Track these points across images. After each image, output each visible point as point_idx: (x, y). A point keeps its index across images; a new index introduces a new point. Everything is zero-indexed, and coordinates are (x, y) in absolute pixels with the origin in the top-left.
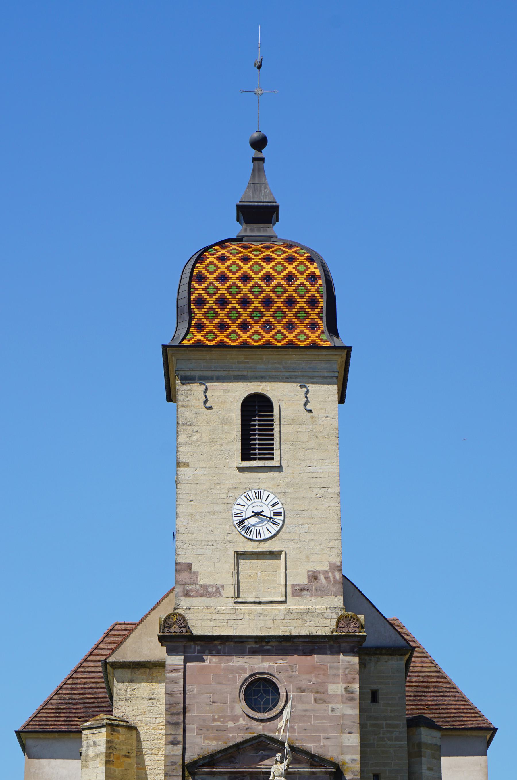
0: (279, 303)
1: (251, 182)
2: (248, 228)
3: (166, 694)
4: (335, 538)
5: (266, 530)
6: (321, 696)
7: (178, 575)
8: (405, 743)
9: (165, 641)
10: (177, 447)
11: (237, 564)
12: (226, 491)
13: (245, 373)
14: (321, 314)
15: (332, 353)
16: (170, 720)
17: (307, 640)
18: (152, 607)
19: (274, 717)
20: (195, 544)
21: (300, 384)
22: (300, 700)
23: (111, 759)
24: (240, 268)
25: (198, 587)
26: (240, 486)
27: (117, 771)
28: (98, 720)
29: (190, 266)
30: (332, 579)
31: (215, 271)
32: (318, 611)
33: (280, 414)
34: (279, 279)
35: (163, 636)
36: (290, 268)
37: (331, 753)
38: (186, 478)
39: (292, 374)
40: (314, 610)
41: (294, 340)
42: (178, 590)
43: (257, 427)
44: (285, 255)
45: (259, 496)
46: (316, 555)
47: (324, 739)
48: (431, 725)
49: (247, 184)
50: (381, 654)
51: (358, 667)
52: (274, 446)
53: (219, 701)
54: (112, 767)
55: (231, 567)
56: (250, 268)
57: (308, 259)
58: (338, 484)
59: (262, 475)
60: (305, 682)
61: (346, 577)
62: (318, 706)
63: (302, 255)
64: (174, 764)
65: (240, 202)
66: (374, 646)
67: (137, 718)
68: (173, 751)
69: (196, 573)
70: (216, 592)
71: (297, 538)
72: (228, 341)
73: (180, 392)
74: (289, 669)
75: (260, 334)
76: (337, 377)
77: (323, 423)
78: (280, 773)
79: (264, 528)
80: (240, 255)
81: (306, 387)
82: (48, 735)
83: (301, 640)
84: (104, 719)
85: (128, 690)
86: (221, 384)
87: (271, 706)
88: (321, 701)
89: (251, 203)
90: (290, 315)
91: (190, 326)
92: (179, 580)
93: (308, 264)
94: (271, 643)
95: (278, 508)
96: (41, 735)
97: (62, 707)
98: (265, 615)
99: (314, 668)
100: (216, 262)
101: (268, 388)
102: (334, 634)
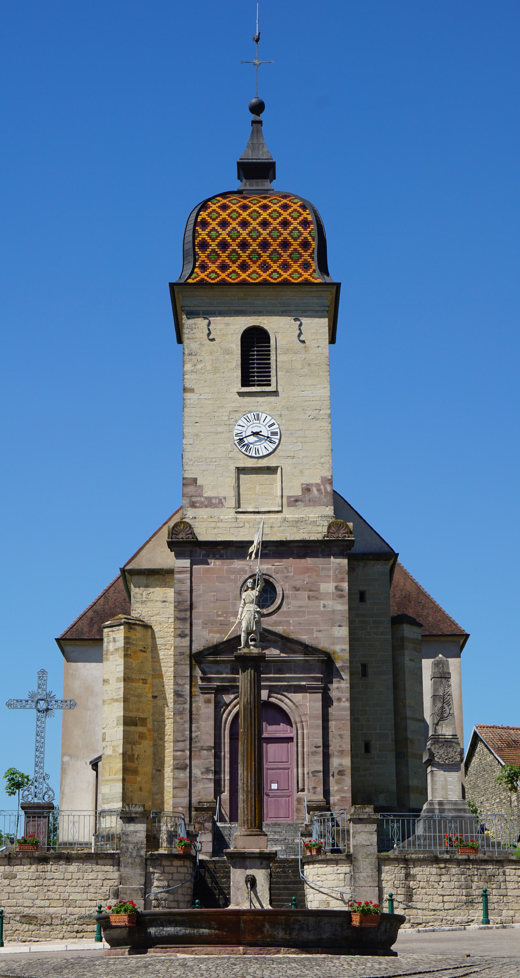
0: (275, 245)
1: (250, 143)
2: (248, 183)
3: (175, 593)
4: (326, 455)
5: (264, 448)
6: (314, 594)
7: (185, 489)
8: (389, 637)
9: (173, 546)
10: (184, 375)
11: (238, 479)
12: (228, 414)
13: (244, 308)
14: (313, 255)
16: (178, 616)
17: (301, 544)
18: (165, 522)
19: (272, 612)
20: (200, 461)
21: (294, 318)
22: (295, 597)
23: (129, 653)
24: (240, 215)
25: (203, 499)
26: (240, 409)
27: (134, 663)
28: (117, 619)
29: (194, 214)
30: (323, 491)
31: (217, 218)
32: (311, 519)
34: (275, 224)
35: (171, 542)
36: (285, 214)
37: (323, 644)
38: (191, 402)
39: (287, 308)
40: (307, 518)
41: (289, 278)
42: (186, 502)
43: (255, 357)
44: (280, 204)
45: (258, 418)
46: (309, 470)
47: (317, 631)
48: (413, 622)
49: (246, 145)
51: (347, 568)
52: (271, 374)
54: (130, 660)
55: (232, 481)
56: (249, 215)
57: (301, 206)
58: (328, 407)
59: (260, 399)
61: (336, 493)
62: (311, 603)
63: (295, 203)
64: (182, 654)
65: (240, 159)
66: (360, 551)
67: (152, 619)
68: (181, 642)
69: (201, 487)
70: (220, 503)
71: (292, 455)
72: (228, 279)
73: (186, 326)
74: (285, 571)
75: (257, 273)
76: (328, 311)
77: (315, 352)
78: (251, 599)
79: (262, 446)
80: (239, 204)
81: (299, 320)
82: (83, 643)
83: (296, 544)
84: (122, 619)
85: (144, 594)
86: (222, 318)
87: (269, 603)
88: (314, 599)
89: (250, 161)
90: (285, 256)
91: (194, 267)
92: (185, 493)
93: (301, 211)
94: (269, 548)
95: (275, 428)
96: (78, 643)
97: (96, 619)
99: (308, 570)
100: (218, 210)
101: (266, 322)
102: (326, 538)
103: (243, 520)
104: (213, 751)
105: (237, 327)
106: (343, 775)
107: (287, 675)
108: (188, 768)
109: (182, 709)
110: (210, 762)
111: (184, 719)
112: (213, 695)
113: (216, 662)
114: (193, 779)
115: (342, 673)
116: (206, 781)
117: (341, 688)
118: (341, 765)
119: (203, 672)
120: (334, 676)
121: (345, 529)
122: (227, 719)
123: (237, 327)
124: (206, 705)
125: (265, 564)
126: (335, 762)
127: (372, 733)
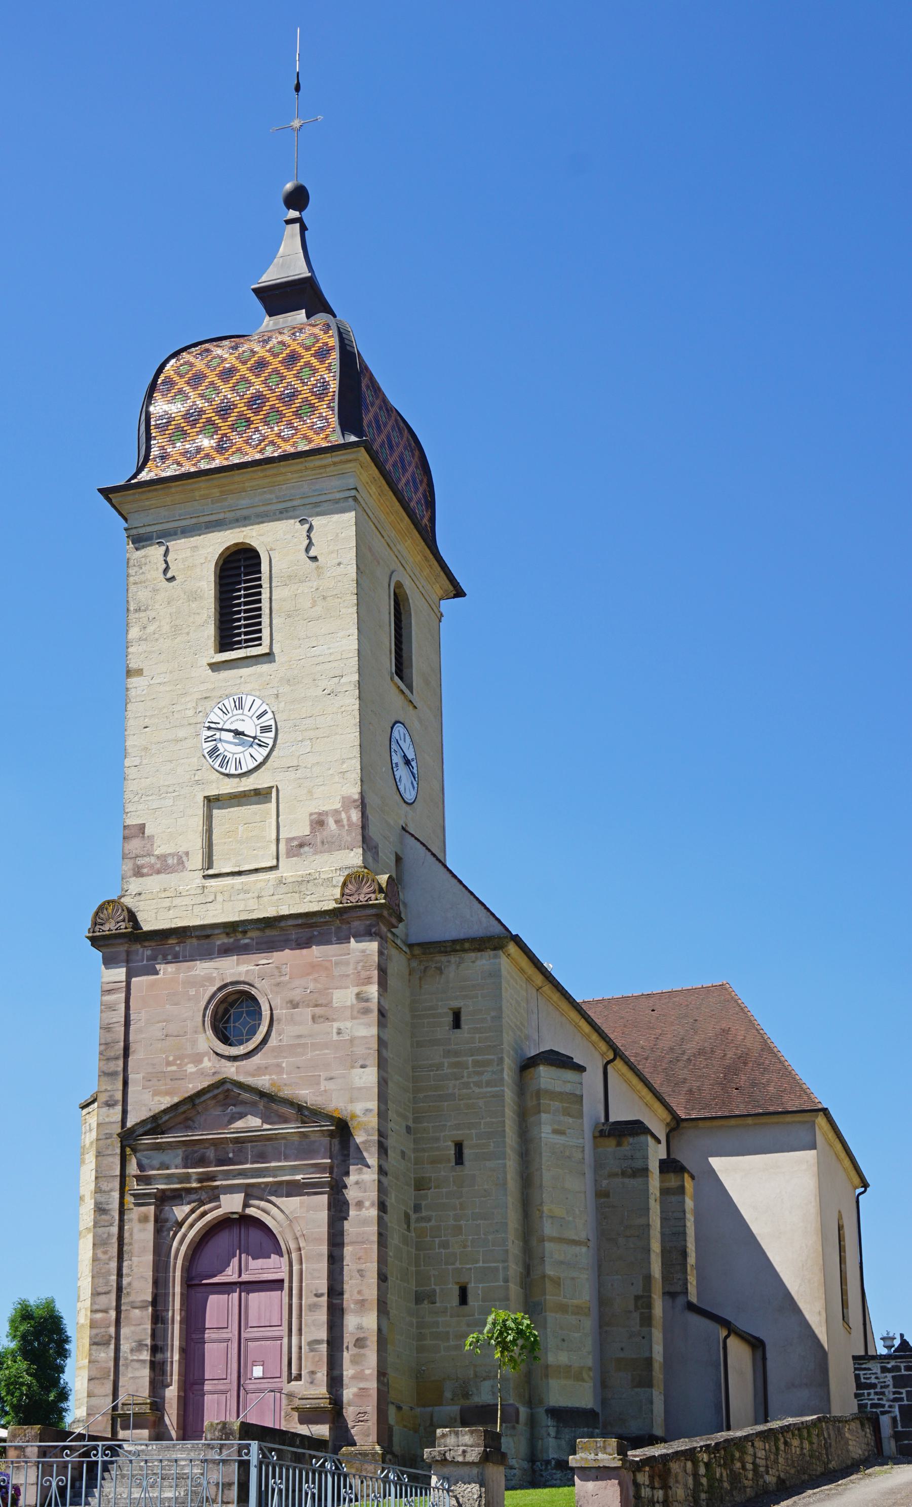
4: (351, 755)
5: (248, 757)
7: (126, 845)
10: (128, 648)
12: (194, 705)
13: (221, 516)
15: (343, 458)
16: (105, 1069)
17: (300, 921)
25: (153, 860)
30: (345, 822)
32: (323, 876)
33: (271, 571)
37: (336, 1102)
38: (139, 692)
39: (289, 504)
43: (242, 600)
45: (239, 705)
46: (323, 787)
50: (464, 950)
53: (176, 1033)
55: (197, 822)
59: (244, 671)
60: (298, 991)
64: (109, 1136)
68: (108, 1116)
74: (276, 973)
77: (334, 574)
94: (249, 934)
98: (247, 892)
101: (254, 534)
103: (213, 890)
104: (150, 1309)
105: (210, 550)
106: (363, 1347)
107: (273, 1164)
108: (113, 1341)
109: (106, 1235)
110: (145, 1329)
111: (110, 1254)
112: (152, 1208)
113: (158, 1147)
114: (121, 1362)
115: (365, 1154)
116: (137, 1365)
117: (362, 1183)
118: (360, 1328)
119: (141, 1166)
120: (351, 1161)
121: (370, 886)
122: (178, 1250)
123: (210, 550)
124: (141, 1226)
125: (244, 963)
126: (351, 1322)
127: (471, 1269)
